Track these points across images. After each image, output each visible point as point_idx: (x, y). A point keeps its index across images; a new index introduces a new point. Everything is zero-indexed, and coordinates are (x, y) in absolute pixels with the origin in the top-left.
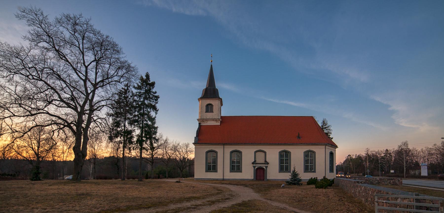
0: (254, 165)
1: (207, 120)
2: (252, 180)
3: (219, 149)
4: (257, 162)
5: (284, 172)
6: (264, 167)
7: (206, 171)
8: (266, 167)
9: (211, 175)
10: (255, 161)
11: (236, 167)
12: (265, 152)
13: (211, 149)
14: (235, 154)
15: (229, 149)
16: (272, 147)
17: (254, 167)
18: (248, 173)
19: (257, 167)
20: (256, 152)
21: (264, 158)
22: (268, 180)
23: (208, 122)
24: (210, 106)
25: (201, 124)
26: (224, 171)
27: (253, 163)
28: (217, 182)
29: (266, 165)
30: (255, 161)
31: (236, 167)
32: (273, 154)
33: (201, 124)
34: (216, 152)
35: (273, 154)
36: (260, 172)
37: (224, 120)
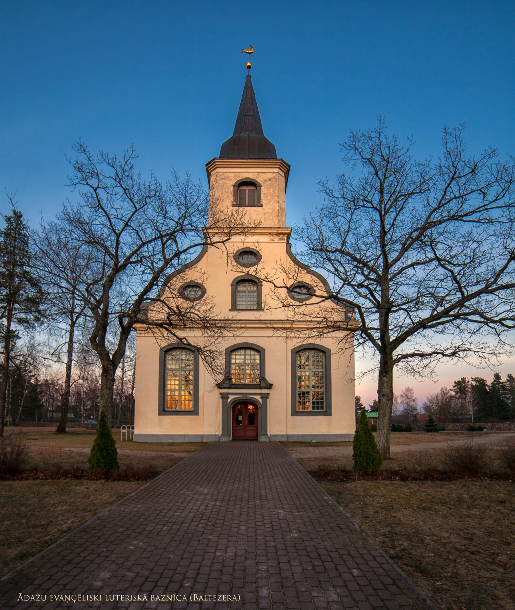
6: (258, 398)
8: (265, 397)
17: (224, 397)
19: (231, 397)
29: (264, 391)
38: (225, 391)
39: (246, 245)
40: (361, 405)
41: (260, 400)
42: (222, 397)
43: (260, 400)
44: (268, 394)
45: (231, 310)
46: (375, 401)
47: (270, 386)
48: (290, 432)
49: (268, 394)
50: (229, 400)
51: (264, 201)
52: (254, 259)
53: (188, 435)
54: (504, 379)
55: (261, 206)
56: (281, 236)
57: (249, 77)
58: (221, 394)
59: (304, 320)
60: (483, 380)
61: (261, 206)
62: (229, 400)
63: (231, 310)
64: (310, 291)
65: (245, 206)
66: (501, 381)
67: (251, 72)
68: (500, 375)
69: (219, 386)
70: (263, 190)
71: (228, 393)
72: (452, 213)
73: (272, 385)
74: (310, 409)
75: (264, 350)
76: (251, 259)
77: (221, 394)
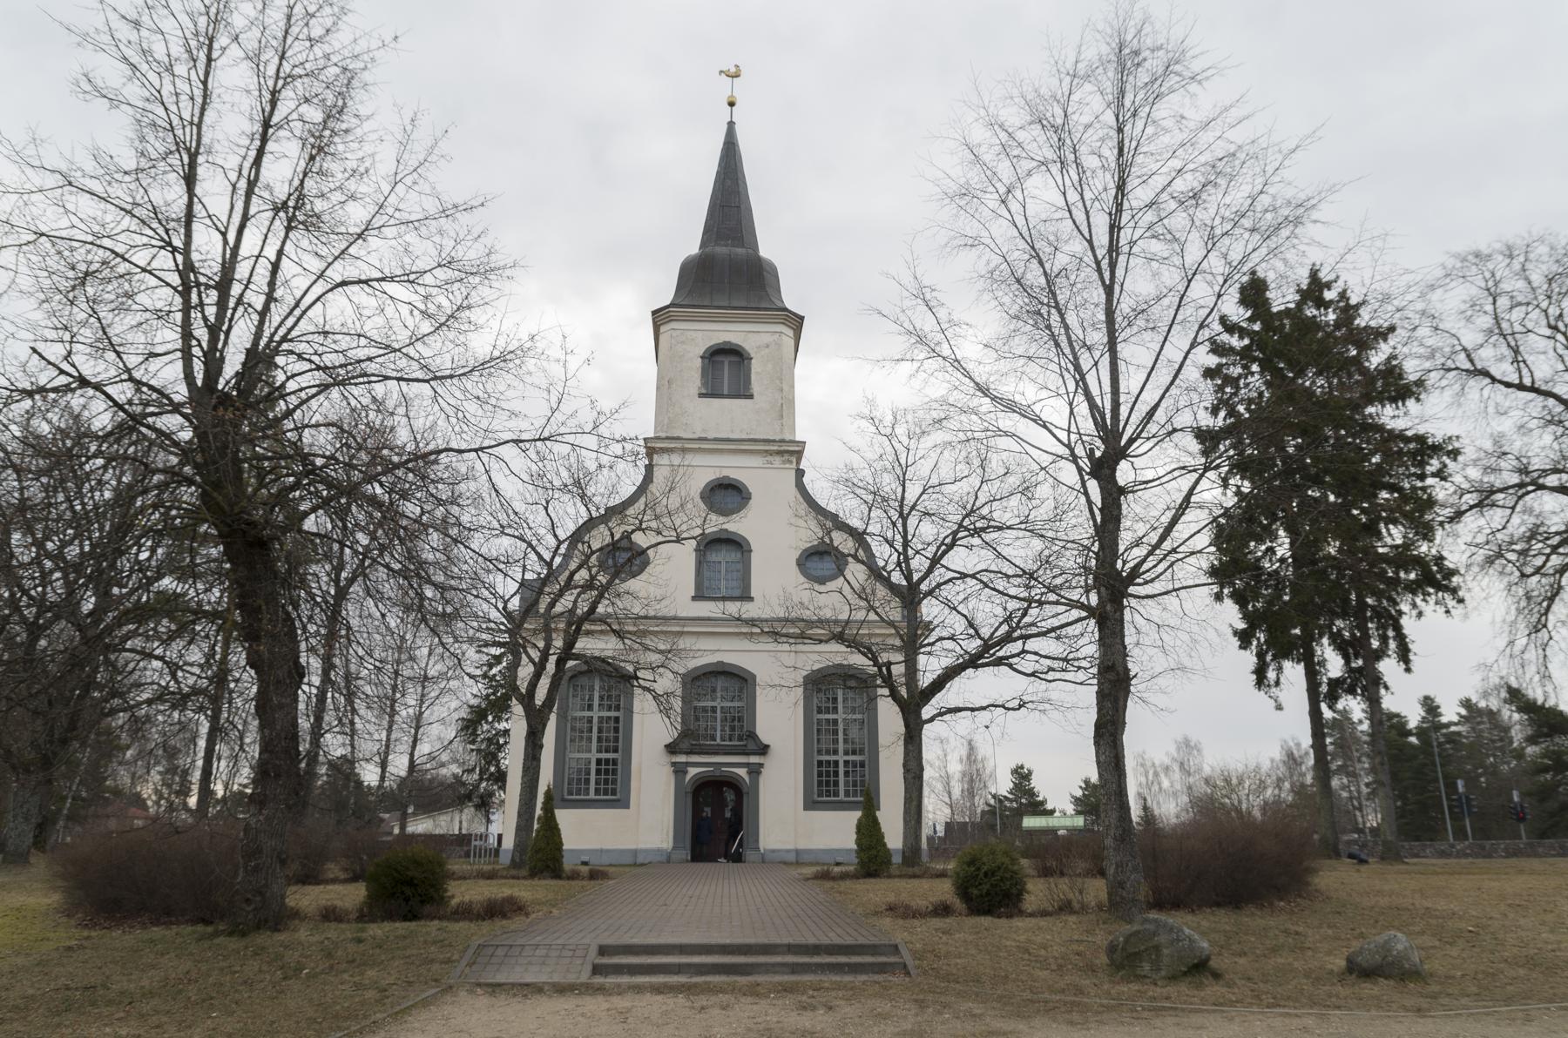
6: (742, 772)
8: (755, 771)
17: (679, 770)
19: (692, 771)
24: (726, 361)
29: (754, 759)
38: (682, 759)
39: (726, 473)
40: (1031, 793)
41: (747, 779)
42: (676, 772)
43: (747, 779)
44: (761, 765)
45: (694, 598)
46: (1087, 782)
47: (764, 750)
48: (802, 845)
49: (761, 765)
50: (688, 777)
51: (756, 386)
52: (737, 499)
53: (608, 851)
54: (1450, 713)
55: (751, 397)
56: (786, 457)
57: (731, 124)
58: (674, 764)
59: (1106, 359)
60: (1398, 715)
61: (751, 397)
62: (688, 777)
63: (694, 598)
64: (840, 560)
65: (721, 396)
66: (1444, 720)
67: (740, 88)
68: (1438, 701)
69: (671, 749)
70: (755, 366)
71: (688, 764)
72: (969, 507)
73: (767, 747)
74: (842, 796)
75: (754, 677)
76: (731, 499)
77: (674, 764)
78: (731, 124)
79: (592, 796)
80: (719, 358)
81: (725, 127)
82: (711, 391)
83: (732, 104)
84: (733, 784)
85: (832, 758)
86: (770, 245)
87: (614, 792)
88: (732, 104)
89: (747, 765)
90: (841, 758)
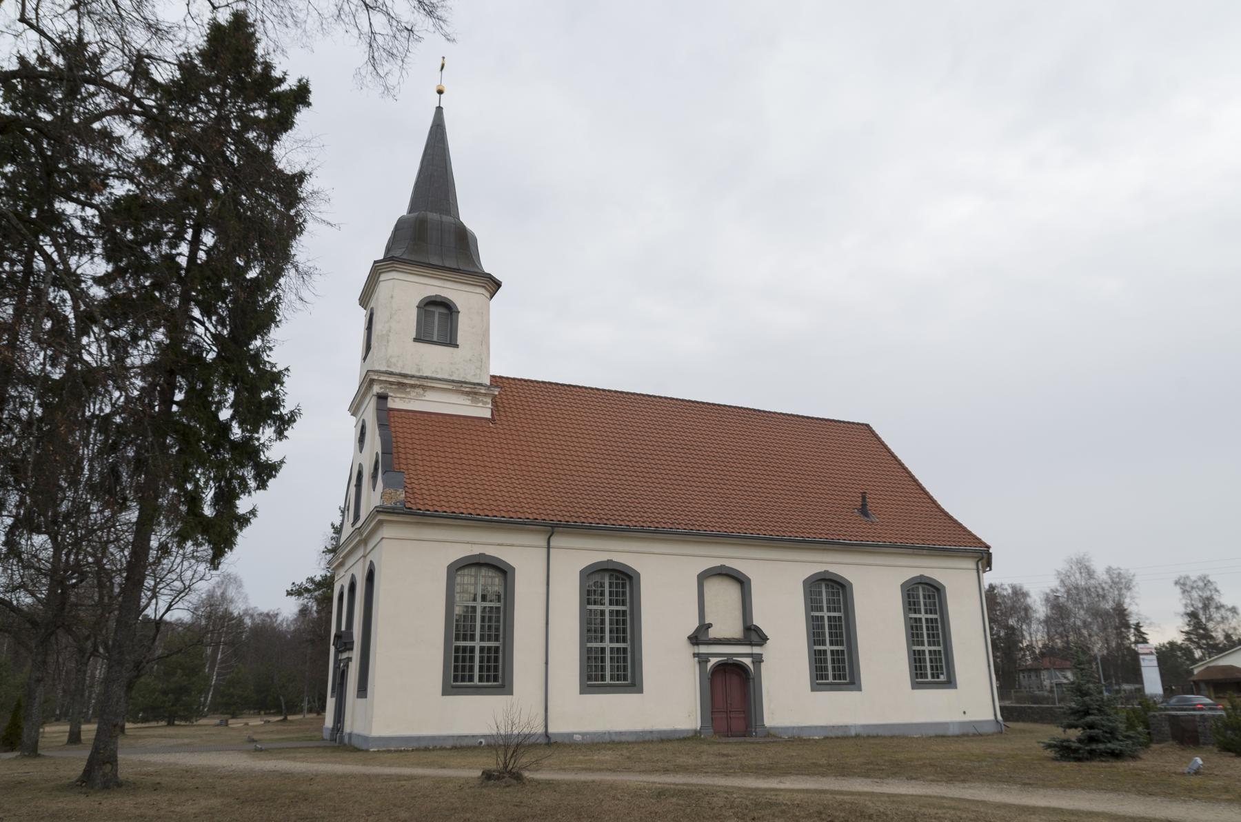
0: (703, 649)
1: (423, 383)
2: (692, 738)
3: (522, 554)
4: (713, 633)
5: (477, 691)
6: (747, 661)
7: (448, 690)
8: (758, 660)
9: (478, 715)
10: (704, 627)
11: (611, 659)
12: (742, 582)
13: (476, 550)
14: (472, 582)
15: (575, 557)
16: (428, 533)
17: (702, 659)
18: (669, 697)
19: (713, 661)
20: (704, 577)
21: (738, 614)
22: (772, 737)
23: (430, 396)
24: (438, 311)
25: (392, 404)
26: (546, 690)
27: (695, 640)
28: (607, 756)
29: (756, 650)
30: (704, 627)
31: (611, 659)
32: (779, 590)
33: (392, 404)
34: (504, 572)
35: (779, 590)
36: (731, 686)
37: (509, 393)
41: (751, 667)
43: (751, 667)
50: (710, 665)
55: (457, 346)
57: (439, 109)
61: (457, 346)
62: (710, 665)
78: (439, 109)
79: (608, 681)
80: (432, 309)
81: (434, 110)
82: (422, 337)
83: (440, 92)
84: (742, 668)
85: (469, 644)
86: (470, 214)
87: (496, 679)
88: (440, 92)
89: (751, 655)
90: (477, 644)
